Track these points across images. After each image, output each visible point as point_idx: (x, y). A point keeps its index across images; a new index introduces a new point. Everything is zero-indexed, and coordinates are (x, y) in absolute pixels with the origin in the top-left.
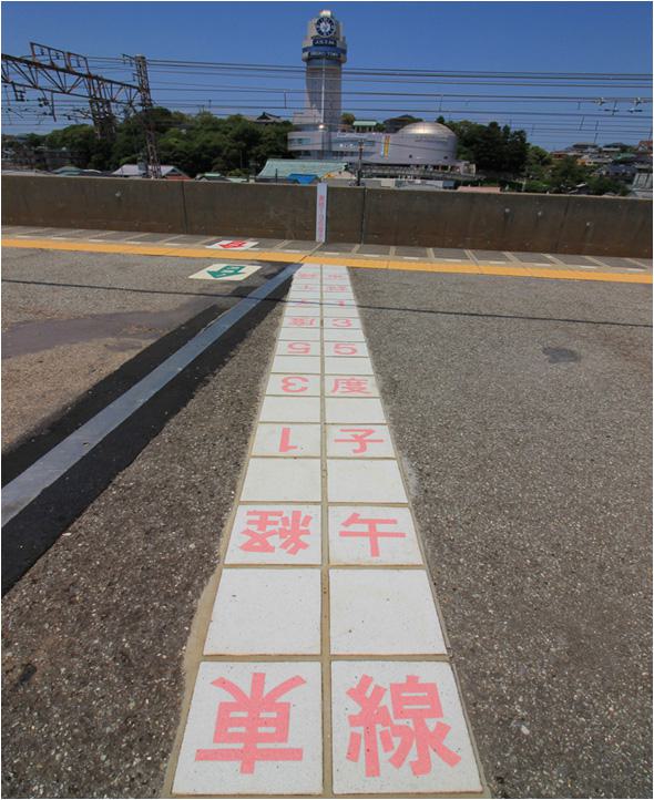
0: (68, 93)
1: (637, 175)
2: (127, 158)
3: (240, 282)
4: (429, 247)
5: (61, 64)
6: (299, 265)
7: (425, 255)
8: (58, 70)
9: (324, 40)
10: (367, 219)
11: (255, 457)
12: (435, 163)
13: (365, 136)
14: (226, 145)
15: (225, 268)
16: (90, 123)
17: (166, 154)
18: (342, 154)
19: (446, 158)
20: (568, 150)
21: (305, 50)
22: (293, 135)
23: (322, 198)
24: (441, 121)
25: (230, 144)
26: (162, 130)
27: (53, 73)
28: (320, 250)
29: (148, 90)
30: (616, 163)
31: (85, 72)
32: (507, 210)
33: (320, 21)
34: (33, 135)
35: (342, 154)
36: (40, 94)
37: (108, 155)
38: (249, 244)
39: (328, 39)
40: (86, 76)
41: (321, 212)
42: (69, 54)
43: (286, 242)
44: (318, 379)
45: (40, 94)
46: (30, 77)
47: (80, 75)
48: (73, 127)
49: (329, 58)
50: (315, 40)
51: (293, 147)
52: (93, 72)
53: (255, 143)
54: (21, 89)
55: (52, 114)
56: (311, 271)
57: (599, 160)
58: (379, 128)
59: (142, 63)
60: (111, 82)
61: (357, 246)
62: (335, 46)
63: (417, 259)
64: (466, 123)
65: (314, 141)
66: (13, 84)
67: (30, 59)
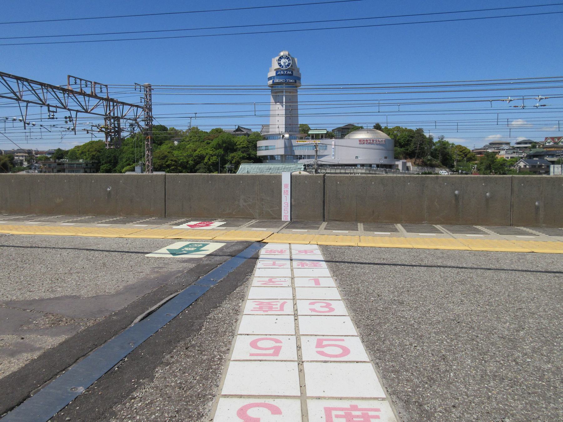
0: (89, 113)
1: (552, 166)
2: (128, 167)
3: (201, 259)
4: (398, 223)
5: (88, 91)
6: (262, 243)
7: (396, 230)
8: (84, 94)
9: (283, 71)
10: (327, 201)
11: (225, 396)
12: (378, 163)
13: (318, 142)
14: (207, 154)
15: (187, 246)
16: (101, 137)
17: (159, 162)
18: (300, 157)
19: (386, 158)
20: (486, 147)
21: (270, 78)
22: (260, 143)
23: (286, 186)
24: (378, 127)
25: (211, 152)
26: (158, 142)
27: (81, 98)
28: (287, 227)
29: (150, 110)
30: (530, 157)
31: (105, 97)
32: (456, 192)
33: (281, 58)
34: (59, 150)
35: (300, 157)
36: (67, 114)
37: (115, 164)
38: (216, 224)
39: (287, 70)
40: (105, 99)
41: (286, 200)
42: (95, 83)
43: (254, 222)
44: (298, 403)
45: (67, 114)
46: (63, 101)
47: (102, 99)
48: (92, 143)
49: (287, 83)
50: (277, 71)
51: (260, 153)
52: (110, 97)
53: (233, 150)
54: (54, 109)
55: (74, 129)
56: (279, 247)
57: (515, 155)
58: (329, 136)
59: (149, 88)
60: (124, 104)
61: (324, 224)
62: (291, 75)
63: (389, 233)
64: (398, 129)
65: (277, 148)
66: (48, 106)
67: (66, 87)
